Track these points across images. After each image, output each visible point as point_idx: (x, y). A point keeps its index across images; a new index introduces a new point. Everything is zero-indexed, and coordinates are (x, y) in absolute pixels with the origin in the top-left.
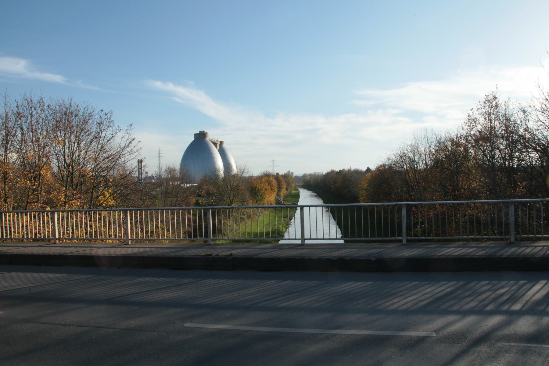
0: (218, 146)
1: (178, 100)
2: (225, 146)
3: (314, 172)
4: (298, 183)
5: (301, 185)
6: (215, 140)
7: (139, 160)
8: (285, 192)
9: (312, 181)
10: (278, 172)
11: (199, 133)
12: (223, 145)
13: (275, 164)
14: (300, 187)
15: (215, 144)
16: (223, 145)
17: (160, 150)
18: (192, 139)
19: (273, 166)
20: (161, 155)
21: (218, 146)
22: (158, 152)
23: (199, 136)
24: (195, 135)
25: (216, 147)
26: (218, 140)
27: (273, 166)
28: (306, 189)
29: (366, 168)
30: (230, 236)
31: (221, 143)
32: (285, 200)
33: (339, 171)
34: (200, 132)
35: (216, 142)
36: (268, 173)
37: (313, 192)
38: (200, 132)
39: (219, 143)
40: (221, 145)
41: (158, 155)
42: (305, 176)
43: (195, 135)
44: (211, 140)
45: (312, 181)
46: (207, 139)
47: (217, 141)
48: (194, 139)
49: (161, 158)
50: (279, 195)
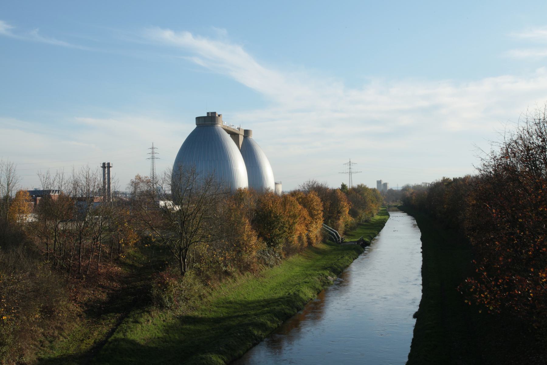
0: (241, 139)
1: (198, 61)
2: (253, 137)
3: (423, 183)
4: (393, 201)
5: (399, 205)
6: (234, 127)
7: (104, 164)
8: (350, 219)
9: (414, 198)
10: (345, 183)
11: (206, 115)
12: (250, 137)
13: (354, 168)
14: (396, 208)
15: (234, 135)
16: (250, 137)
17: (155, 146)
18: (192, 126)
19: (350, 173)
20: (155, 155)
21: (241, 139)
22: (150, 151)
23: (205, 122)
24: (198, 119)
25: (237, 142)
26: (241, 128)
27: (350, 173)
28: (405, 212)
29: (380, 180)
30: (183, 310)
31: (247, 133)
32: (349, 233)
33: (452, 179)
34: (208, 113)
35: (237, 132)
36: (363, 186)
37: (413, 218)
38: (208, 113)
39: (242, 133)
40: (247, 136)
41: (150, 156)
42: (406, 189)
43: (198, 119)
44: (226, 128)
45: (414, 198)
46: (219, 126)
47: (239, 129)
48: (196, 126)
49: (156, 160)
50: (335, 224)
